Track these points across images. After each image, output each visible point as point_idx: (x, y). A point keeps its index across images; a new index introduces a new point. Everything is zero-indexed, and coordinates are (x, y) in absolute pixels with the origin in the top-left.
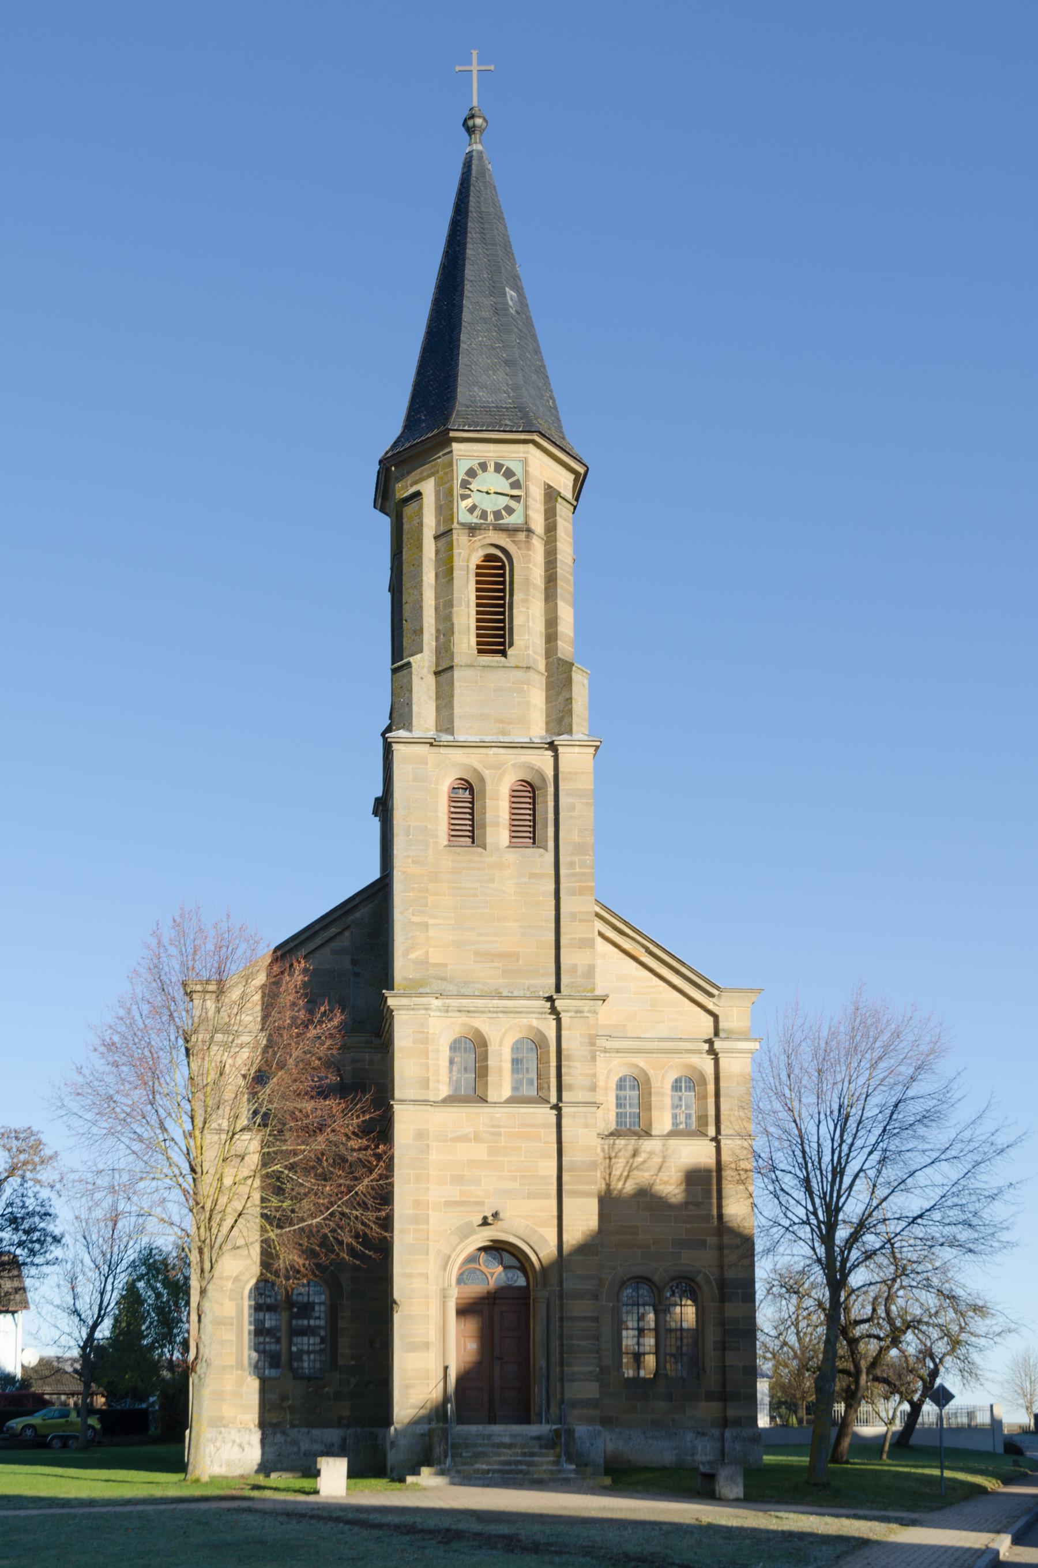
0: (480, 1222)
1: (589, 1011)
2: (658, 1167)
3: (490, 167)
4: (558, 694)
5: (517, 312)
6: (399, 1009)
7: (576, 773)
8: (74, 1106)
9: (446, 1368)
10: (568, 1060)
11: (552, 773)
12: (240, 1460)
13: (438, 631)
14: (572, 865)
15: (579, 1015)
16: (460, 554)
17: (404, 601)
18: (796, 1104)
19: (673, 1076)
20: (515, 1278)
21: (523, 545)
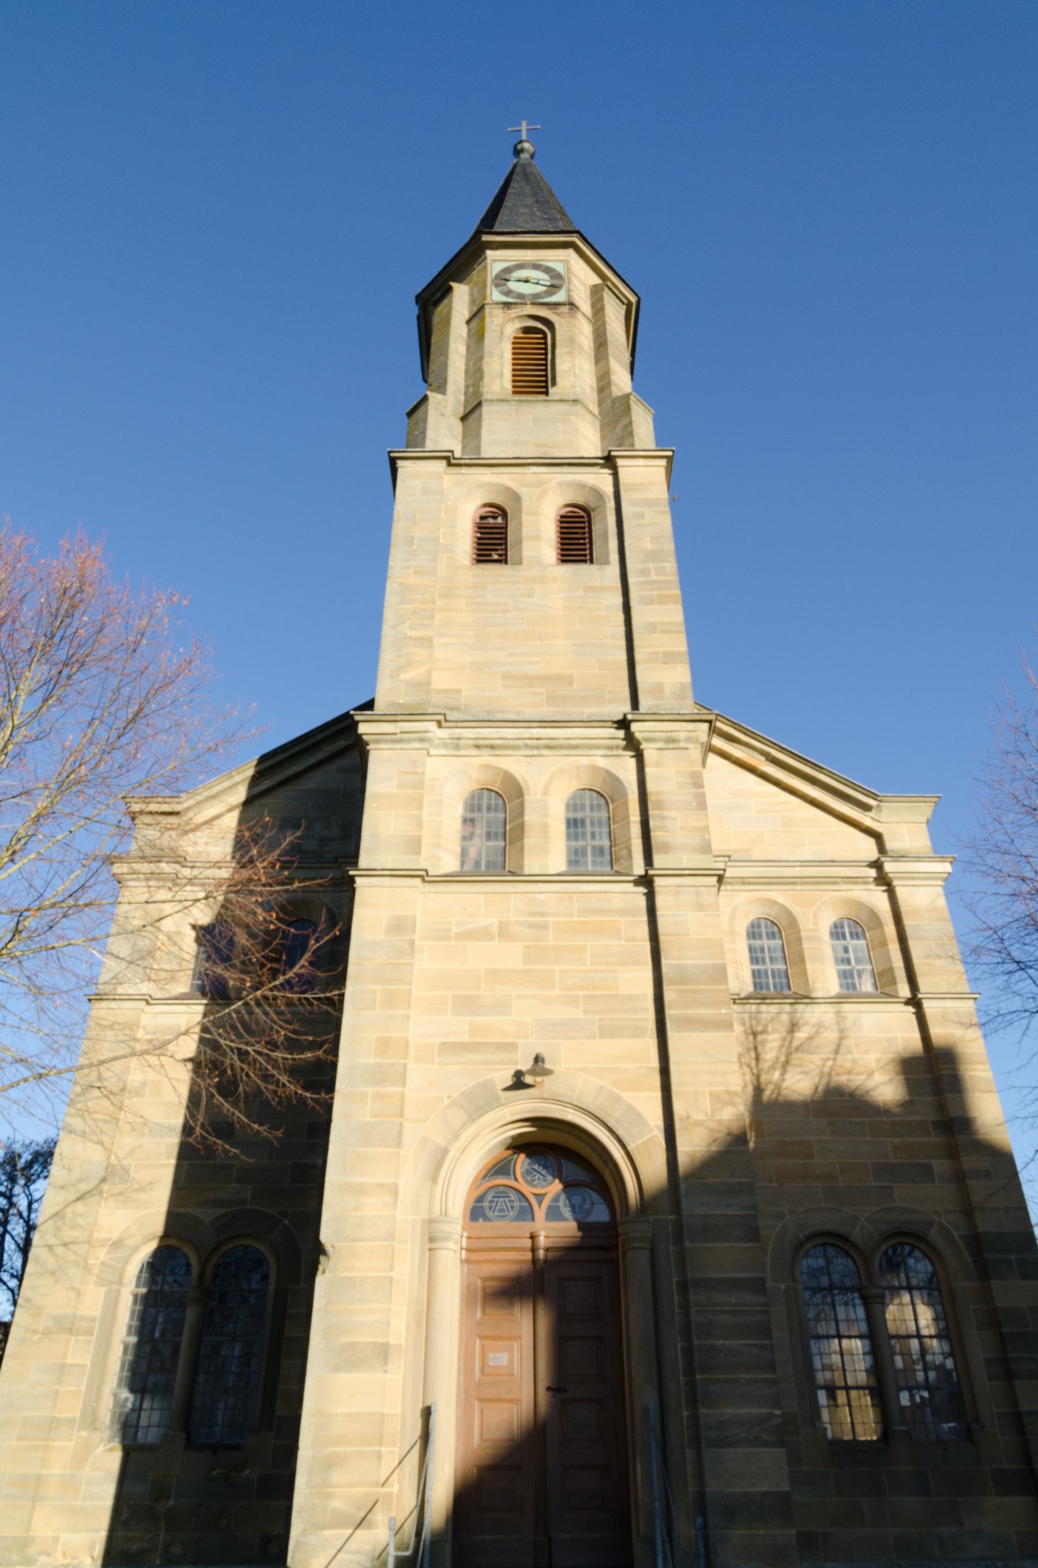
0: (509, 1082)
1: (689, 740)
2: (833, 1048)
6: (377, 742)
7: (643, 484)
9: (427, 1413)
14: (645, 572)
15: (671, 746)
16: (493, 322)
20: (587, 1206)
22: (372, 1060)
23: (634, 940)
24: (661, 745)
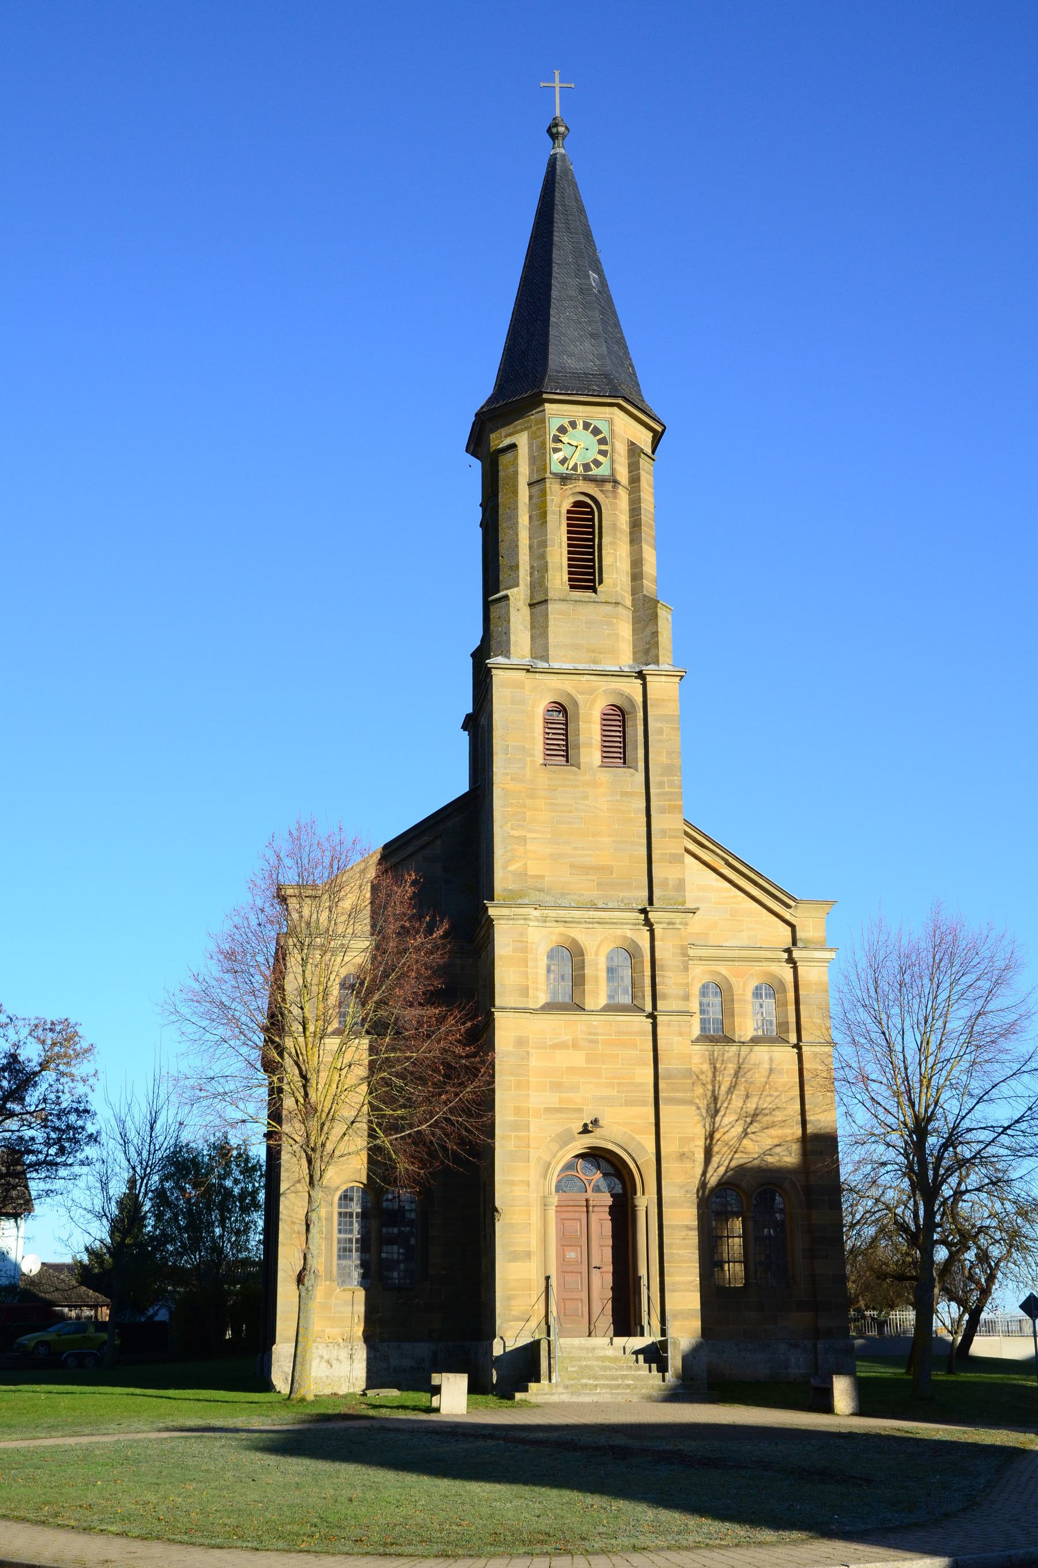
1: (681, 923)
3: (572, 167)
4: (645, 628)
5: (599, 291)
7: (663, 700)
8: (185, 1011)
9: (548, 1278)
10: (662, 970)
11: (641, 699)
12: (327, 1377)
13: (532, 567)
14: (661, 784)
16: (553, 500)
17: (500, 540)
18: (884, 1016)
19: (753, 984)
20: (613, 1185)
21: (610, 494)
22: (512, 1118)
23: (644, 1050)
24: (665, 926)
